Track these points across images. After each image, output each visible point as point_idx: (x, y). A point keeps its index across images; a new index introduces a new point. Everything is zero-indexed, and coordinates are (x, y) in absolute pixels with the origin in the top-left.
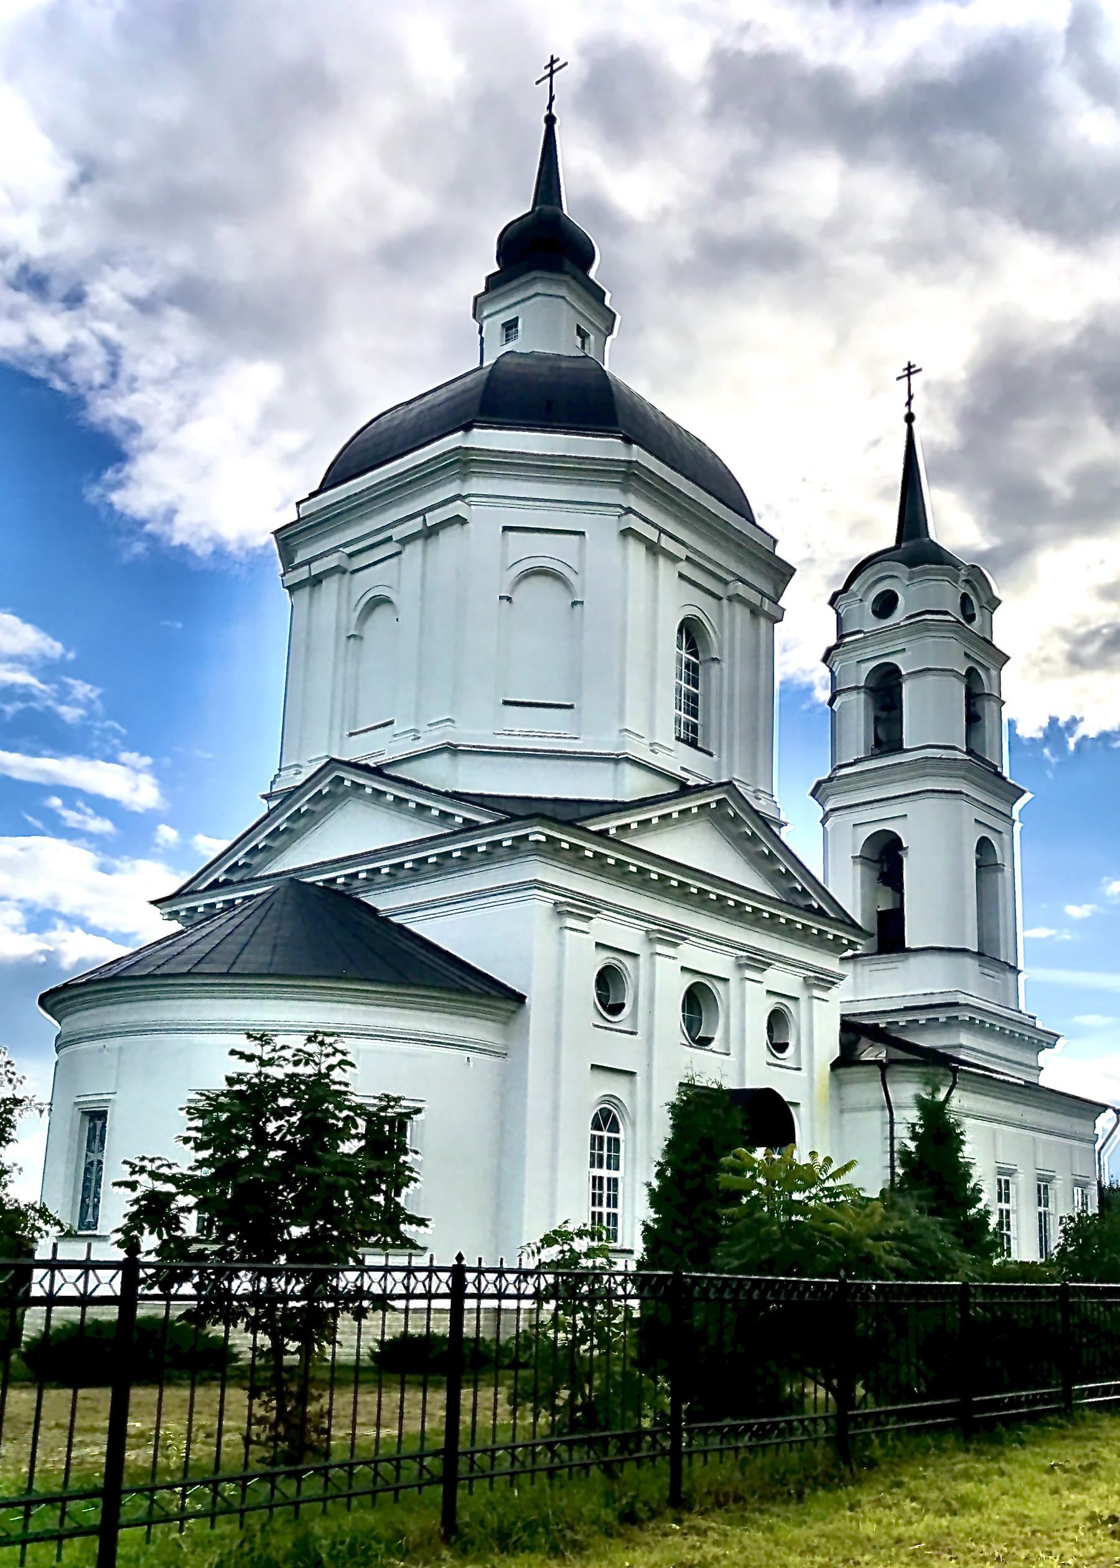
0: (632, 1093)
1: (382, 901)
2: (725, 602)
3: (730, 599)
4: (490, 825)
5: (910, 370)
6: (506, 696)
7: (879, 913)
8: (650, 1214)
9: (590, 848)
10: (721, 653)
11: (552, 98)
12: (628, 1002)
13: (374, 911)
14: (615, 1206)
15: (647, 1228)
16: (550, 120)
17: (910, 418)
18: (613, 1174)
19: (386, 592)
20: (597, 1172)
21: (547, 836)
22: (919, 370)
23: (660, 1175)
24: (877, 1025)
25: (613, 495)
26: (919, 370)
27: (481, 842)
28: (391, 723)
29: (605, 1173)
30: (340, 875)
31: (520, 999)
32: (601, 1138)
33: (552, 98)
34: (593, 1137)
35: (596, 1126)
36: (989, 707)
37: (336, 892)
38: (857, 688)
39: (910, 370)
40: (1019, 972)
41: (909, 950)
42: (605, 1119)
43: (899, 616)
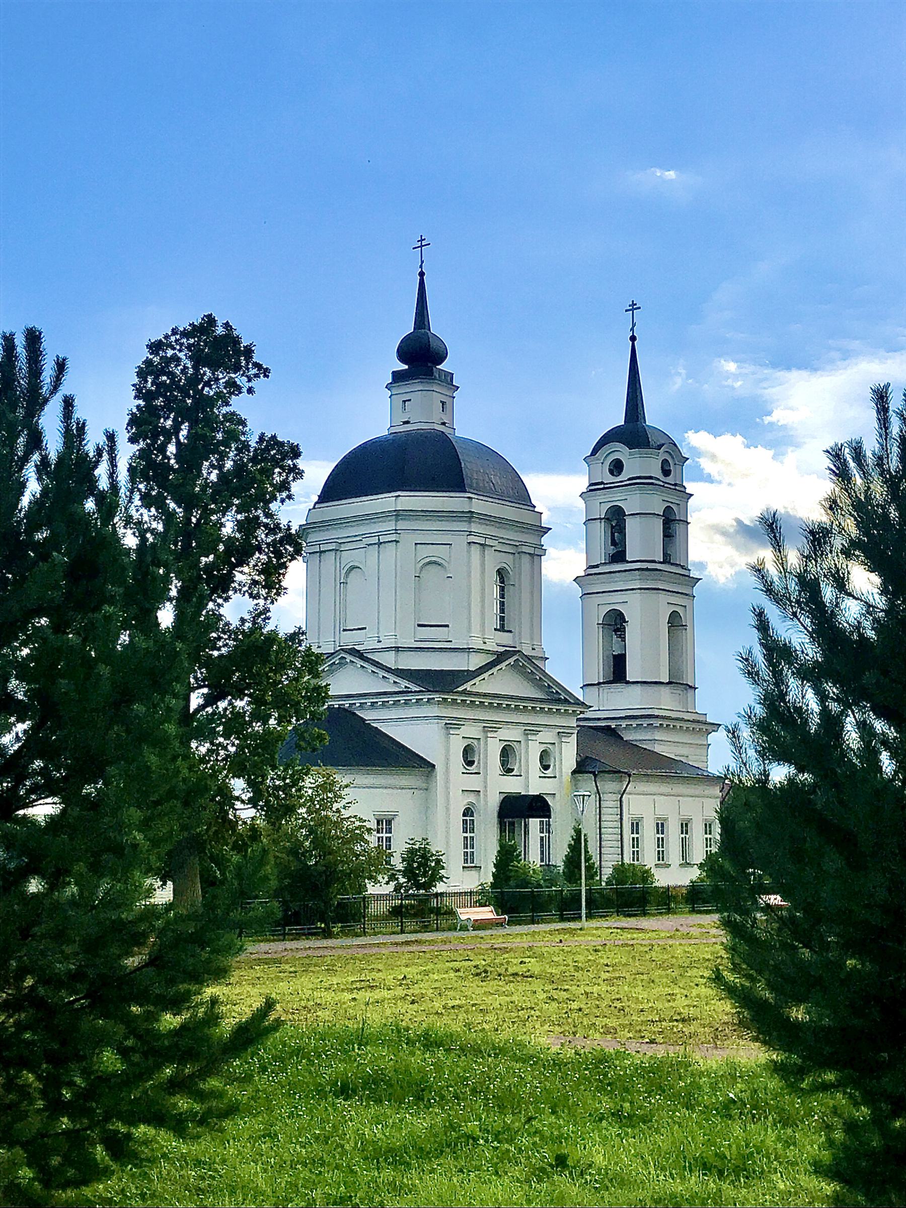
0: (478, 801)
1: (367, 715)
2: (516, 554)
3: (519, 553)
4: (415, 692)
5: (633, 307)
6: (477, 820)
7: (614, 656)
8: (494, 870)
9: (459, 699)
10: (515, 581)
11: (422, 262)
12: (476, 760)
13: (363, 720)
14: (473, 848)
15: (493, 873)
16: (422, 274)
17: (633, 339)
18: (472, 835)
19: (356, 564)
20: (465, 835)
21: (443, 698)
22: (639, 308)
23: (496, 859)
24: (610, 726)
25: (464, 526)
26: (639, 308)
27: (413, 698)
28: (365, 628)
29: (468, 835)
30: (346, 704)
31: (434, 766)
32: (466, 820)
33: (422, 262)
34: (463, 820)
35: (464, 815)
36: (679, 528)
37: (344, 709)
38: (600, 519)
39: (633, 307)
40: (695, 688)
41: (628, 682)
42: (468, 812)
43: (624, 476)
